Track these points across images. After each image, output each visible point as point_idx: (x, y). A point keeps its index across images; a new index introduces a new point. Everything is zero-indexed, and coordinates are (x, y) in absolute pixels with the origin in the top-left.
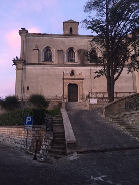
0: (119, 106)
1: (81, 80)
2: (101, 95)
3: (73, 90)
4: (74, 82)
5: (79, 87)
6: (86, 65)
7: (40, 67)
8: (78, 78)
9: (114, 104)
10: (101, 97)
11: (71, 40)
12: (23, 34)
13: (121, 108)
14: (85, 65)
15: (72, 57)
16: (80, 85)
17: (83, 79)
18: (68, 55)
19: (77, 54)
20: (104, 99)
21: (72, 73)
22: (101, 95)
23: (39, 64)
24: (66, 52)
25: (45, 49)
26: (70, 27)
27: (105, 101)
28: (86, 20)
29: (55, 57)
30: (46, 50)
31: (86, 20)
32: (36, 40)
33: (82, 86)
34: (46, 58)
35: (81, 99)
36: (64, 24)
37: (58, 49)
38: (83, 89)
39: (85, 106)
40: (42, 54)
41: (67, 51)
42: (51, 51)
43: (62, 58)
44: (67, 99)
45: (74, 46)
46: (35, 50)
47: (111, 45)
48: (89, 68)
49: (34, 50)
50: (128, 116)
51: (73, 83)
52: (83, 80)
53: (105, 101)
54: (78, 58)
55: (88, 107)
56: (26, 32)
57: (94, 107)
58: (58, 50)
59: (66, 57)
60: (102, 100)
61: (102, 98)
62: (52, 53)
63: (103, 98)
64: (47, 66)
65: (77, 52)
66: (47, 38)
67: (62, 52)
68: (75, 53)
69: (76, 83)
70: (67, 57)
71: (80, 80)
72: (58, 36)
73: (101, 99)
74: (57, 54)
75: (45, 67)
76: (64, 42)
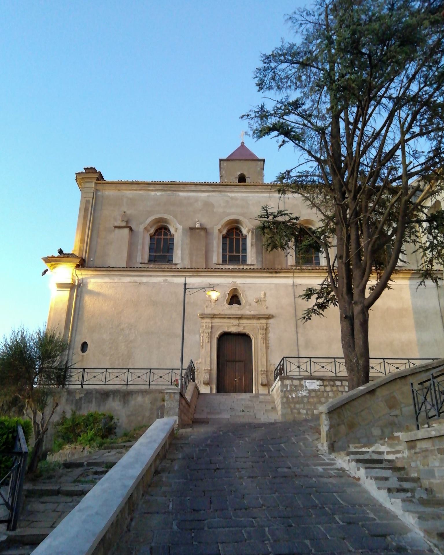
0: (391, 407)
1: (264, 321)
2: (328, 367)
3: (233, 351)
4: (239, 325)
5: (257, 344)
6: (280, 272)
7: (127, 279)
8: (253, 313)
9: (368, 396)
10: (326, 374)
11: (232, 198)
12: (88, 185)
13: (397, 412)
14: (276, 272)
15: (238, 251)
16: (260, 336)
17: (269, 317)
18: (223, 244)
19: (252, 239)
20: (338, 383)
21: (234, 299)
22: (328, 371)
23: (130, 268)
24: (216, 232)
25: (151, 227)
26: (239, 173)
27: (340, 389)
28: (262, 108)
29: (182, 250)
30: (156, 231)
31: (262, 108)
32: (125, 200)
33: (266, 339)
34: (155, 252)
35: (262, 385)
36: (222, 166)
37: (192, 226)
38: (269, 351)
39: (270, 408)
40: (140, 241)
41: (220, 231)
42: (169, 231)
43: (204, 252)
44: (214, 387)
45: (243, 215)
46: (131, 230)
47: (346, 165)
48: (290, 281)
49: (117, 230)
50: (426, 450)
51: (233, 330)
52: (270, 321)
53: (340, 389)
54: (254, 250)
55: (280, 413)
56: (98, 179)
57: (299, 413)
58: (191, 229)
59: (215, 249)
60: (333, 386)
61: (333, 380)
62: (172, 239)
63: (334, 381)
64: (151, 276)
65: (253, 232)
66: (159, 193)
67: (202, 233)
68: (245, 239)
69: (247, 331)
70: (221, 250)
71: (259, 319)
72: (193, 188)
73: (326, 383)
74: (187, 240)
75: (144, 280)
76: (213, 206)
